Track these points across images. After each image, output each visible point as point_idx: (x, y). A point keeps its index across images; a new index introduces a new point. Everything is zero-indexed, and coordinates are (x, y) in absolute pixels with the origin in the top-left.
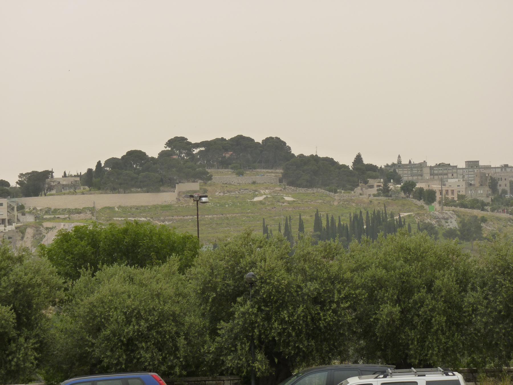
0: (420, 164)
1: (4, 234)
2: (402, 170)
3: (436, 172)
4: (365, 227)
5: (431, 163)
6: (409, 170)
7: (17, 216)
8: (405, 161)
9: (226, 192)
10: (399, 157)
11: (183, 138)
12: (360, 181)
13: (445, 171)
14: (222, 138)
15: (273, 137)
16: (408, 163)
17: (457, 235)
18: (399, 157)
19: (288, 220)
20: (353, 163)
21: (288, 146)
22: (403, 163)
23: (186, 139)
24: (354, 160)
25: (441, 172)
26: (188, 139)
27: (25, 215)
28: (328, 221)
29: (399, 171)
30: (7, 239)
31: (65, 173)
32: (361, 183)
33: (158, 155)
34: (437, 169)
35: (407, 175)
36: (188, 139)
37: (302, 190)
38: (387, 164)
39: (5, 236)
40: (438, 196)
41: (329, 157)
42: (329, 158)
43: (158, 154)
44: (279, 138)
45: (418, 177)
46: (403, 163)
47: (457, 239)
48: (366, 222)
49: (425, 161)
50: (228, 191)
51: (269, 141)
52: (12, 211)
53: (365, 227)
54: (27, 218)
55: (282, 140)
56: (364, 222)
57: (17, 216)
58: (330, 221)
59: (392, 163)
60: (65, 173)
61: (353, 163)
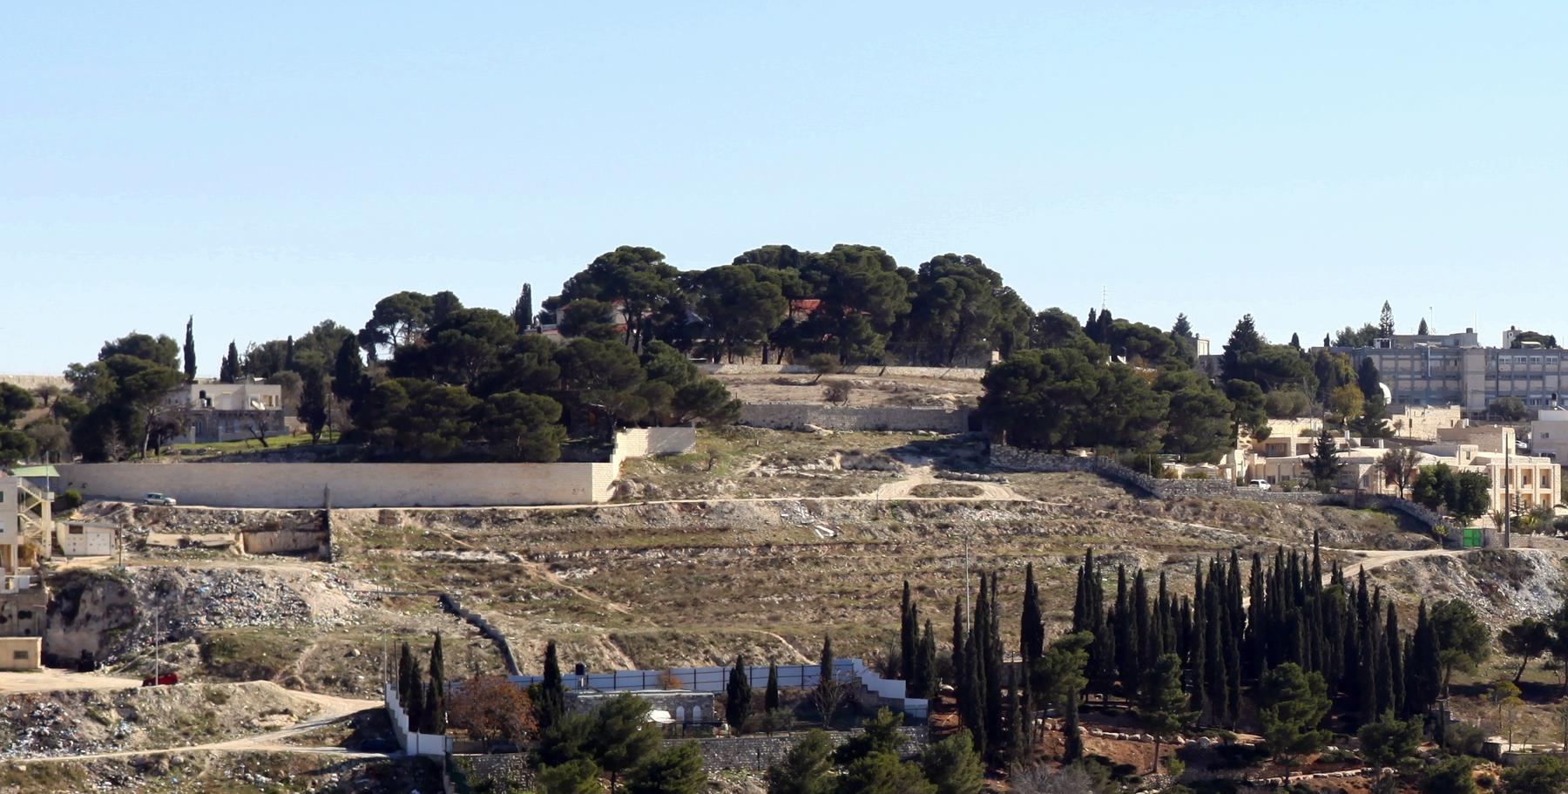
0: (1457, 339)
1: (6, 602)
2: (1393, 356)
3: (1504, 368)
4: (1246, 602)
5: (1491, 338)
6: (1416, 357)
7: (54, 534)
8: (1405, 327)
9: (785, 461)
10: (1387, 307)
11: (649, 251)
12: (1240, 430)
13: (1536, 368)
14: (785, 249)
15: (958, 255)
16: (1416, 332)
17: (1547, 643)
18: (1387, 307)
19: (989, 580)
20: (1224, 347)
21: (1006, 288)
22: (1397, 331)
23: (658, 256)
24: (1231, 340)
25: (1520, 367)
26: (663, 257)
27: (81, 532)
28: (1122, 583)
29: (1382, 359)
30: (15, 619)
31: (232, 347)
32: (1244, 435)
33: (562, 288)
34: (1509, 357)
35: (1409, 376)
36: (663, 257)
37: (1044, 460)
38: (1348, 330)
39: (7, 607)
40: (1496, 494)
41: (1144, 323)
42: (1147, 327)
43: (565, 285)
44: (979, 261)
45: (1444, 383)
46: (1397, 331)
47: (1547, 656)
48: (1251, 587)
49: (1469, 330)
50: (792, 459)
51: (939, 268)
52: (33, 515)
53: (1246, 602)
54: (90, 541)
55: (988, 267)
56: (1245, 584)
57: (54, 534)
58: (1129, 586)
59: (1363, 327)
60: (232, 347)
61: (1224, 347)
